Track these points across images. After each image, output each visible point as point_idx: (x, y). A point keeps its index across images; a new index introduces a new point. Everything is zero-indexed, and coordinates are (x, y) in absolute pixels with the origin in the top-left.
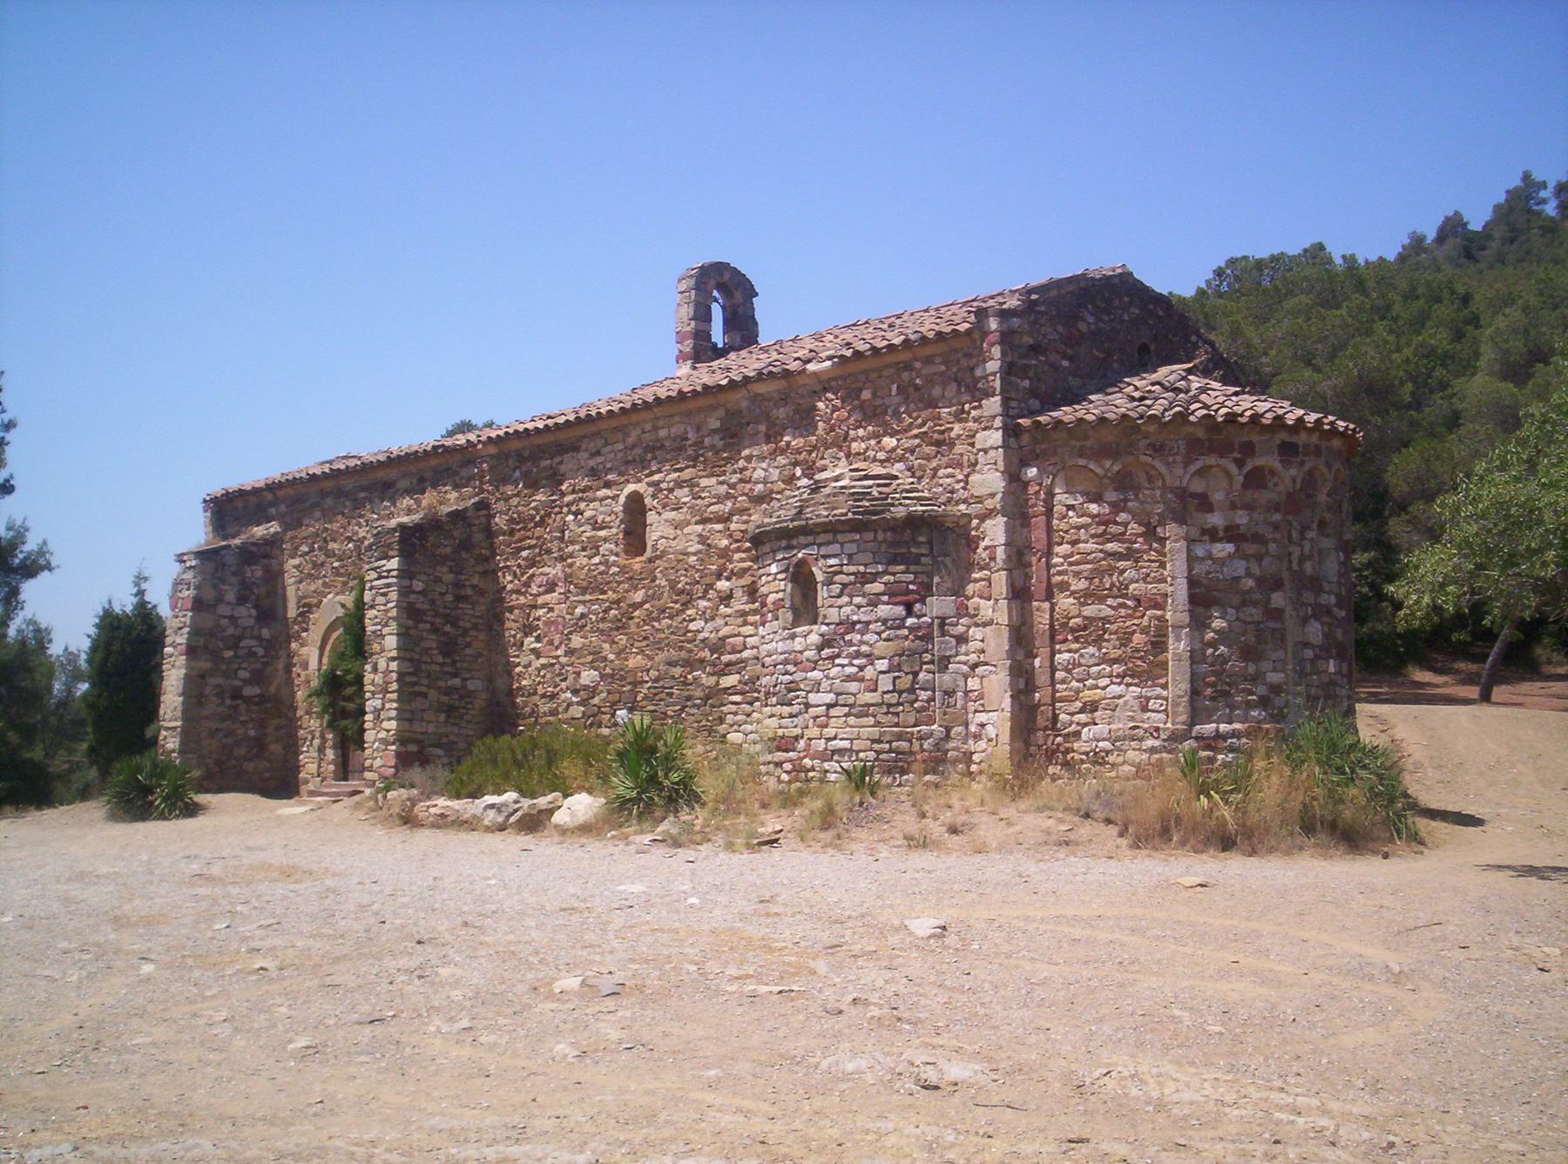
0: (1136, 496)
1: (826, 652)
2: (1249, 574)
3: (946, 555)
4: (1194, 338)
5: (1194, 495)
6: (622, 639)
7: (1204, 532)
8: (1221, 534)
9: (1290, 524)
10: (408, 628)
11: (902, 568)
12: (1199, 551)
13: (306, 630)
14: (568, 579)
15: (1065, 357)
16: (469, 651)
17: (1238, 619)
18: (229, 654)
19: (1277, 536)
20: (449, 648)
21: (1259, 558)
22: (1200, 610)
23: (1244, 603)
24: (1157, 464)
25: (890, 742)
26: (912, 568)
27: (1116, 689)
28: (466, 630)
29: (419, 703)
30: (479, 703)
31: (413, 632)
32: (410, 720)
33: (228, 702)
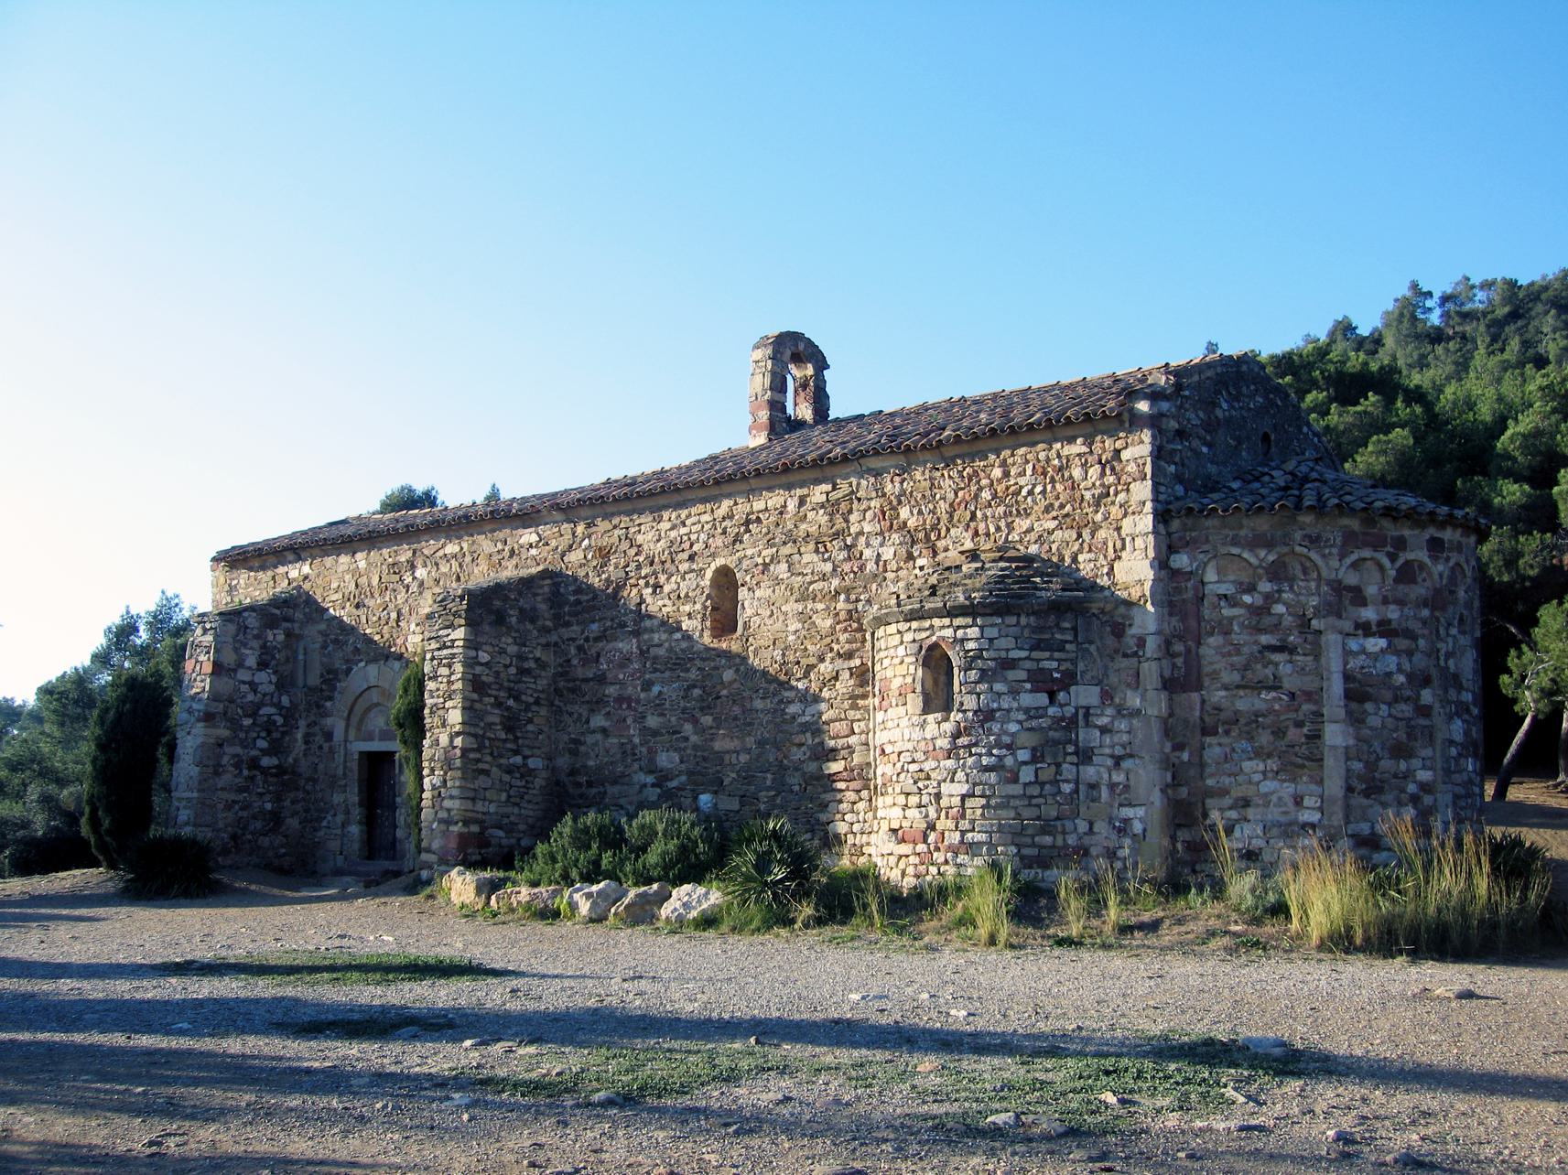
0: (1291, 588)
1: (963, 741)
2: (1400, 670)
3: (1091, 642)
4: (1305, 429)
5: (1350, 589)
6: (707, 720)
7: (1357, 626)
8: (1374, 628)
9: (1438, 620)
10: (473, 701)
11: (1047, 654)
12: (1353, 645)
13: (330, 698)
14: (643, 653)
15: (1205, 443)
16: (530, 727)
17: (1390, 715)
18: (247, 722)
19: (1426, 632)
20: (511, 724)
21: (1410, 653)
22: (1354, 706)
23: (1396, 700)
24: (1314, 555)
25: (1033, 836)
26: (1057, 655)
27: (1268, 786)
28: (528, 706)
29: (482, 781)
30: (539, 782)
31: (478, 706)
32: (473, 799)
33: (246, 772)
